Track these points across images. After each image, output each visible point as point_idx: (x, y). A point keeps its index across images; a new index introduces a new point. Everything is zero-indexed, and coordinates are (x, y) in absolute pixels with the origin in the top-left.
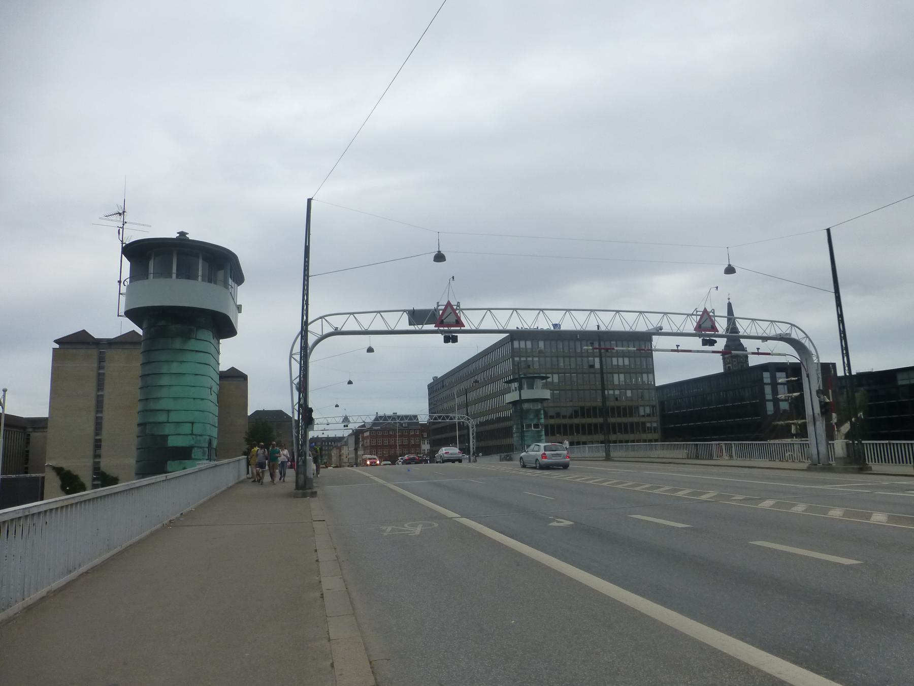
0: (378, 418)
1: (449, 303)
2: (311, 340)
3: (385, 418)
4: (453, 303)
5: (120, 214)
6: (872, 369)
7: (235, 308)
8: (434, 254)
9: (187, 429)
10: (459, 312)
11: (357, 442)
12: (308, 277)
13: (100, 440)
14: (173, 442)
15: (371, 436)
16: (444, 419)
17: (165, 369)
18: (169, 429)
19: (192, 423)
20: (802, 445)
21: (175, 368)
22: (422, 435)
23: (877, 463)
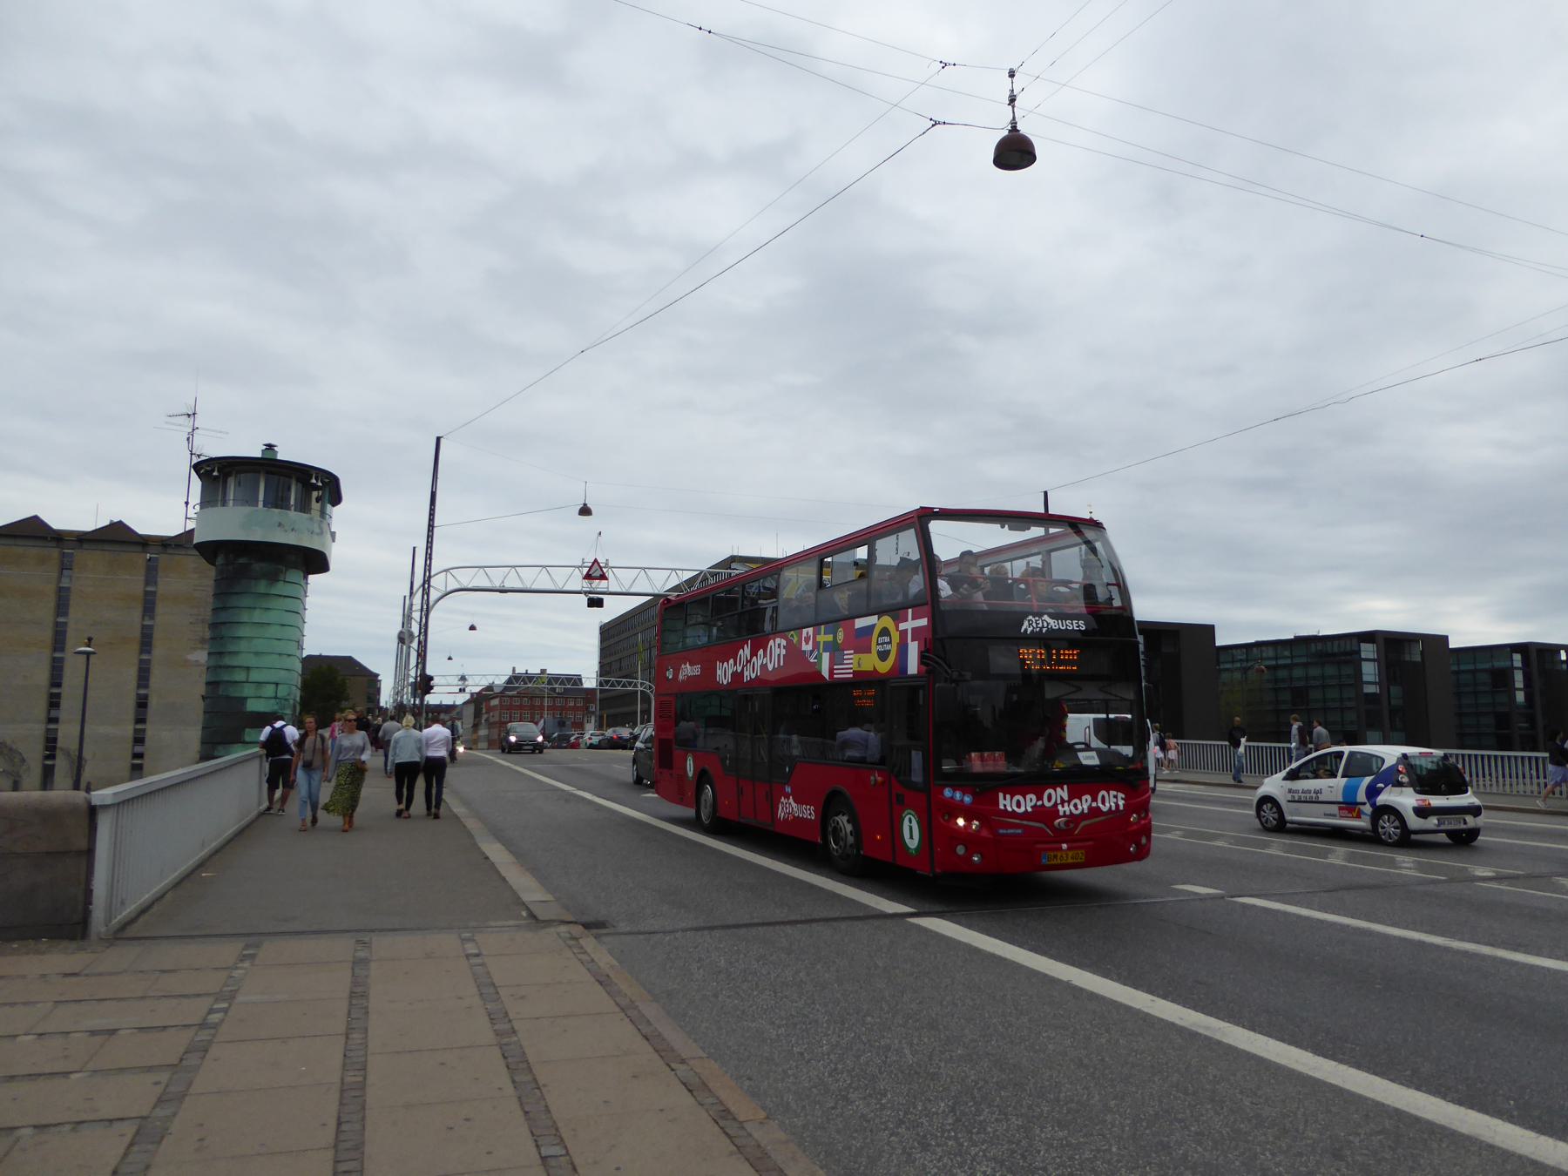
0: (515, 678)
1: (596, 561)
2: (434, 595)
3: (528, 678)
4: (601, 560)
5: (189, 415)
6: (1319, 632)
7: (329, 535)
8: (579, 507)
9: (269, 691)
10: (607, 571)
11: (477, 714)
12: (433, 527)
13: (58, 696)
14: (253, 706)
15: (501, 706)
16: (619, 683)
17: (245, 617)
18: (248, 691)
19: (277, 684)
20: (1479, 759)
21: (257, 616)
22: (587, 708)
23: (1217, 771)
